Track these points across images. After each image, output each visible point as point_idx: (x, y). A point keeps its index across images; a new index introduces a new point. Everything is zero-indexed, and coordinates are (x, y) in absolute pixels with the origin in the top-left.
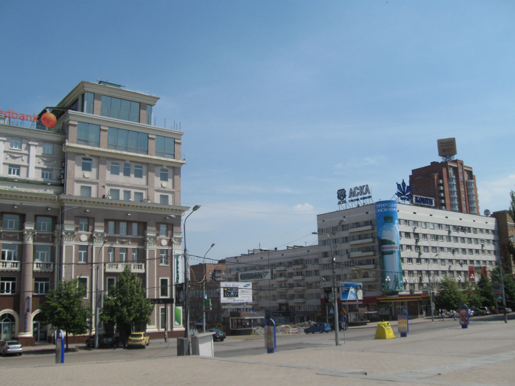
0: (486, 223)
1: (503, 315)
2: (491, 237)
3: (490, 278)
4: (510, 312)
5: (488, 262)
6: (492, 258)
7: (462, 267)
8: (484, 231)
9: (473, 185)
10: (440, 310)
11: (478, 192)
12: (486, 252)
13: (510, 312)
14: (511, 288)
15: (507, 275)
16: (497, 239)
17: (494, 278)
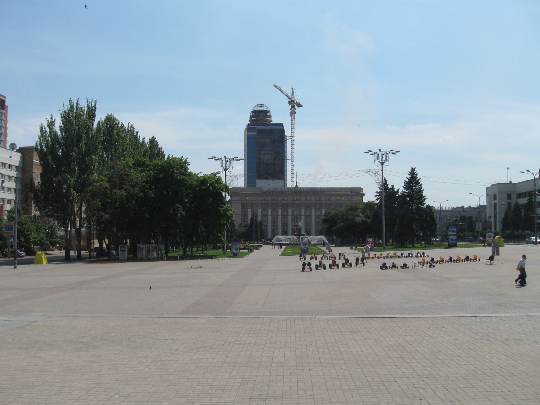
0: (10, 157)
1: (13, 258)
2: (14, 173)
3: (6, 218)
4: (23, 256)
5: (6, 201)
6: (12, 196)
7: (393, 264)
8: (7, 166)
9: (3, 116)
10: (151, 194)
11: (8, 125)
12: (6, 189)
13: (23, 256)
14: (28, 230)
15: (26, 216)
16: (20, 176)
17: (10, 218)
